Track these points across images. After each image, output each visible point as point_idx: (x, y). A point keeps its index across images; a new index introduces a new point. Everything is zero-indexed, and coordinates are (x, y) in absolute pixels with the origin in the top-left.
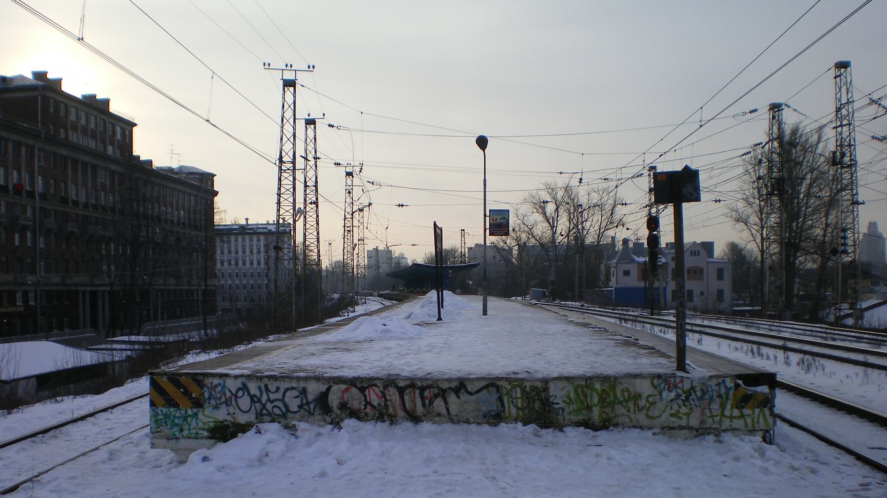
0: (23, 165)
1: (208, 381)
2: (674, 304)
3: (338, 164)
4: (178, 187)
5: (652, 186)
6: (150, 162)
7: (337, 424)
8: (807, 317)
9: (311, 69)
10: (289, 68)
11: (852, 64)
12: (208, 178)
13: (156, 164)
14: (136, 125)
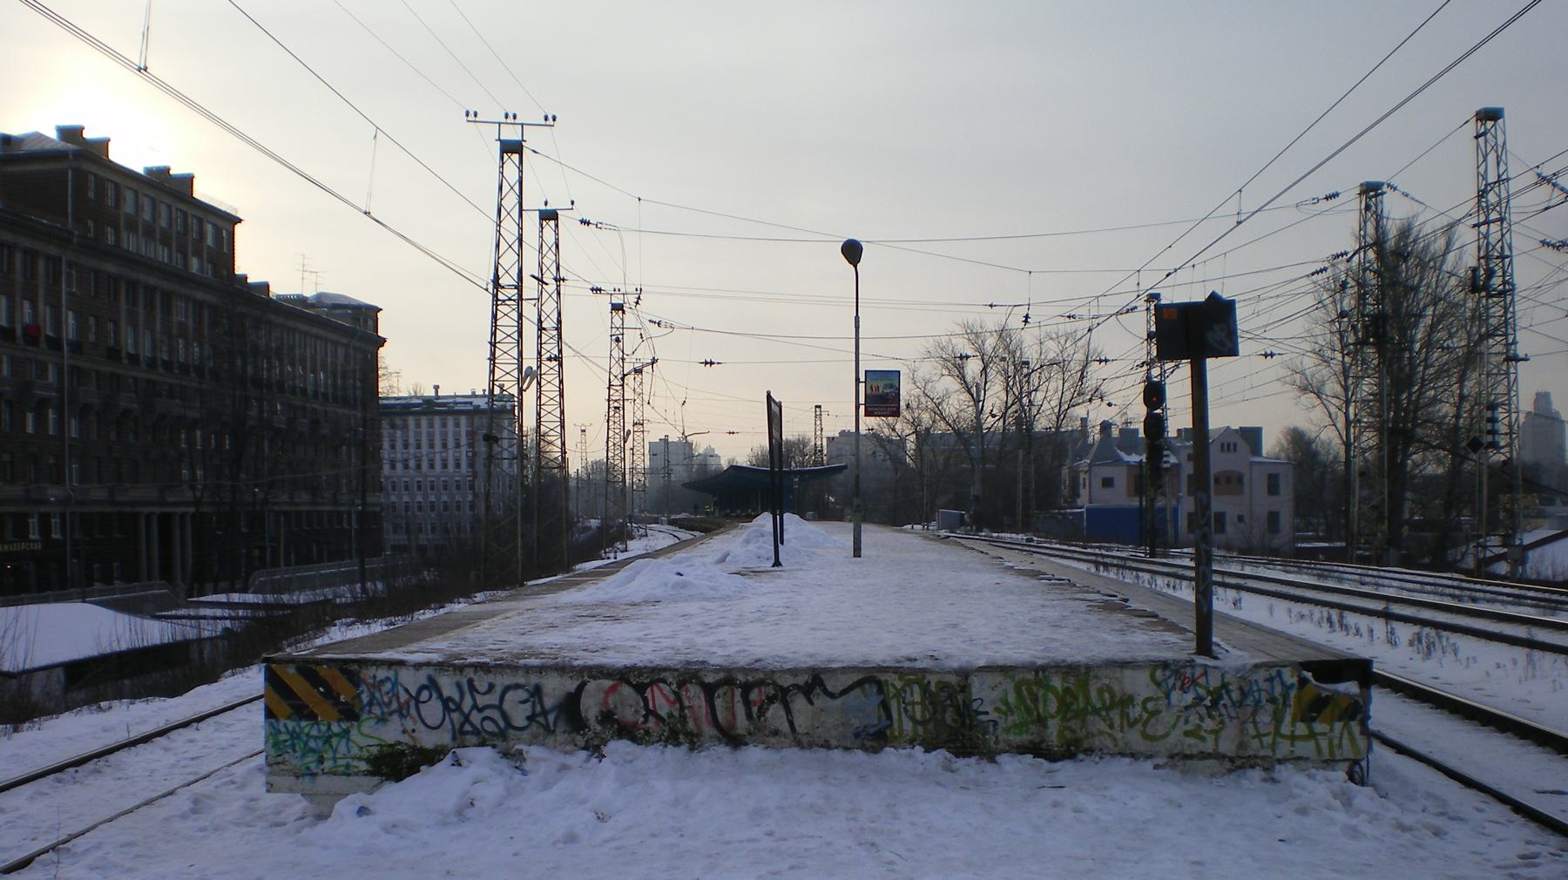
0: (41, 292)
1: (368, 673)
2: (1192, 537)
3: (597, 290)
4: (315, 331)
5: (1153, 329)
6: (265, 287)
7: (595, 749)
8: (1427, 560)
9: (550, 121)
10: (510, 120)
11: (1506, 113)
12: (368, 314)
13: (276, 290)
14: (240, 221)
